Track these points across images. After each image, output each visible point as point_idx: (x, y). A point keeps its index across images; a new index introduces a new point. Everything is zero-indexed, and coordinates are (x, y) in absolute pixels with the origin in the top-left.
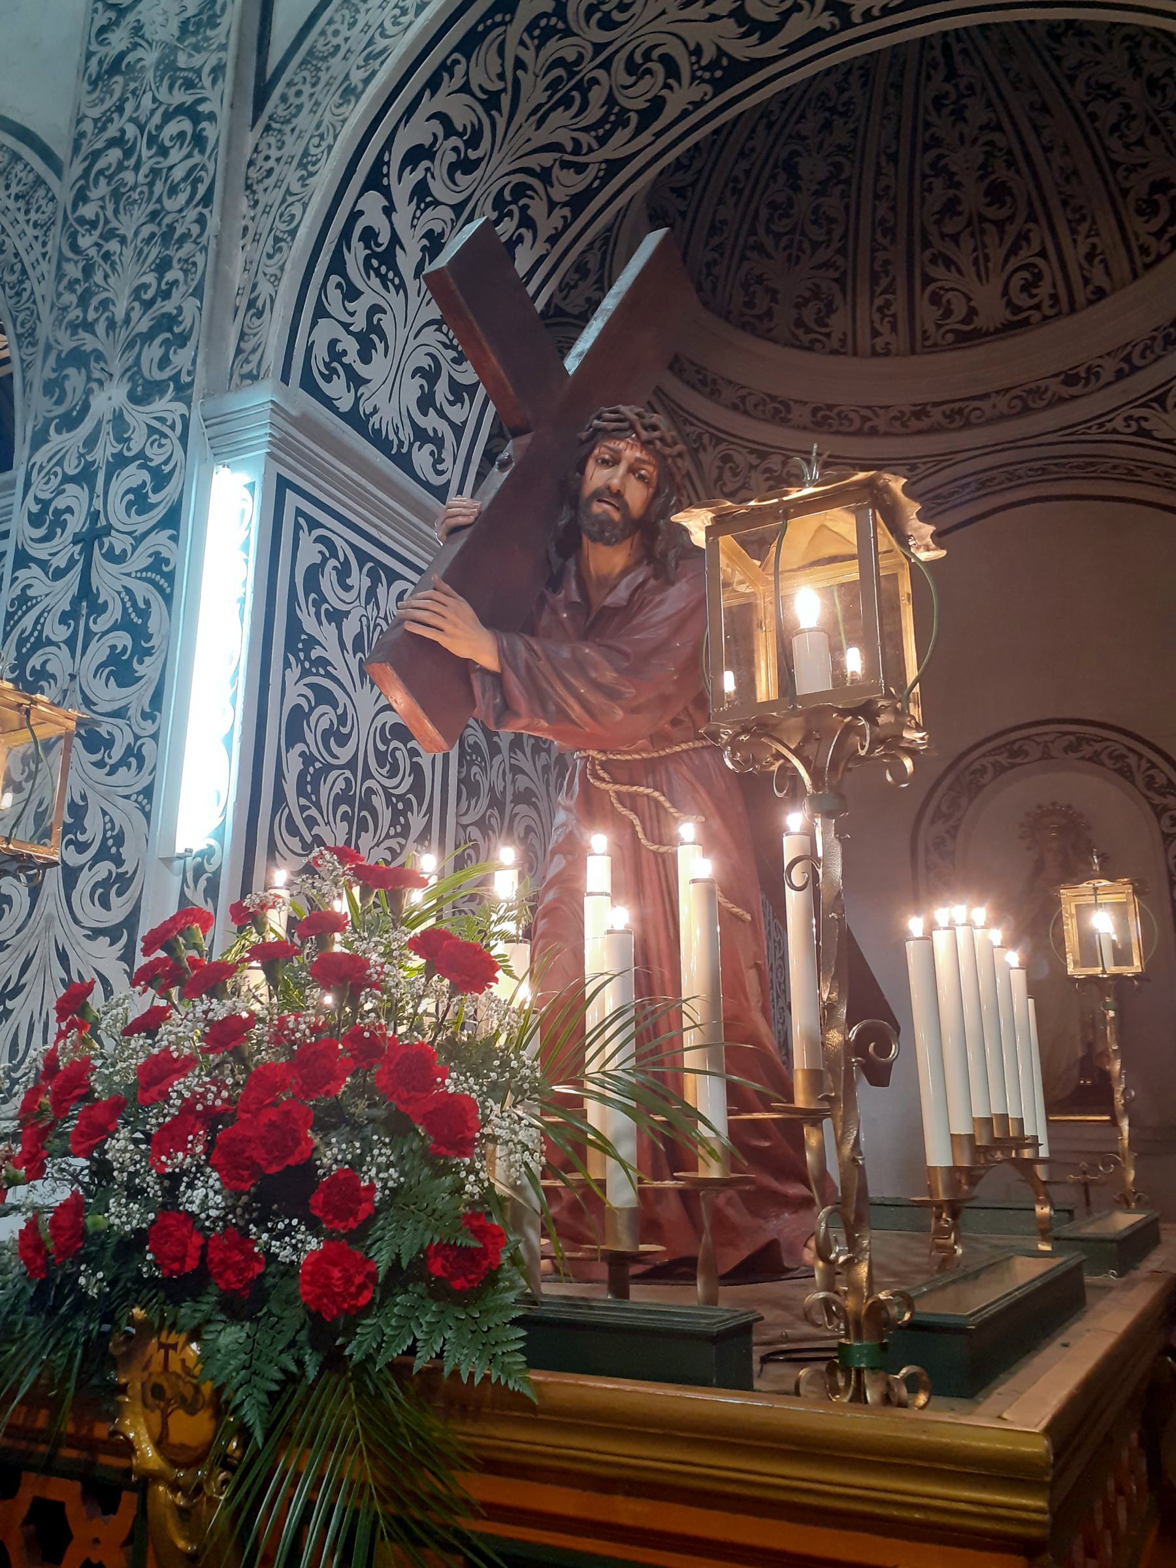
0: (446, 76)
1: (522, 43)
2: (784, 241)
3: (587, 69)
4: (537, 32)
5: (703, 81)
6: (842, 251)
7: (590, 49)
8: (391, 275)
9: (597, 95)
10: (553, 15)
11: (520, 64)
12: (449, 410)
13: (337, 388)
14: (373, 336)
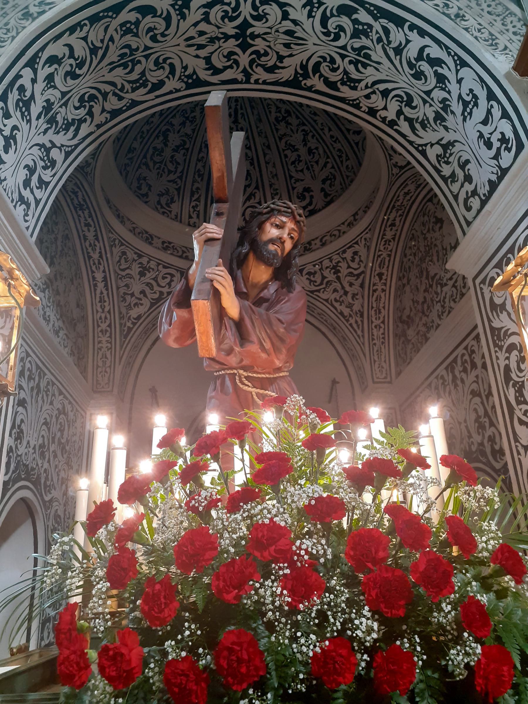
0: (79, 29)
1: (116, 30)
2: (157, 166)
3: (138, 55)
4: (124, 29)
5: (183, 81)
6: (180, 178)
7: (143, 47)
8: (26, 113)
9: (139, 69)
10: (133, 24)
11: (111, 39)
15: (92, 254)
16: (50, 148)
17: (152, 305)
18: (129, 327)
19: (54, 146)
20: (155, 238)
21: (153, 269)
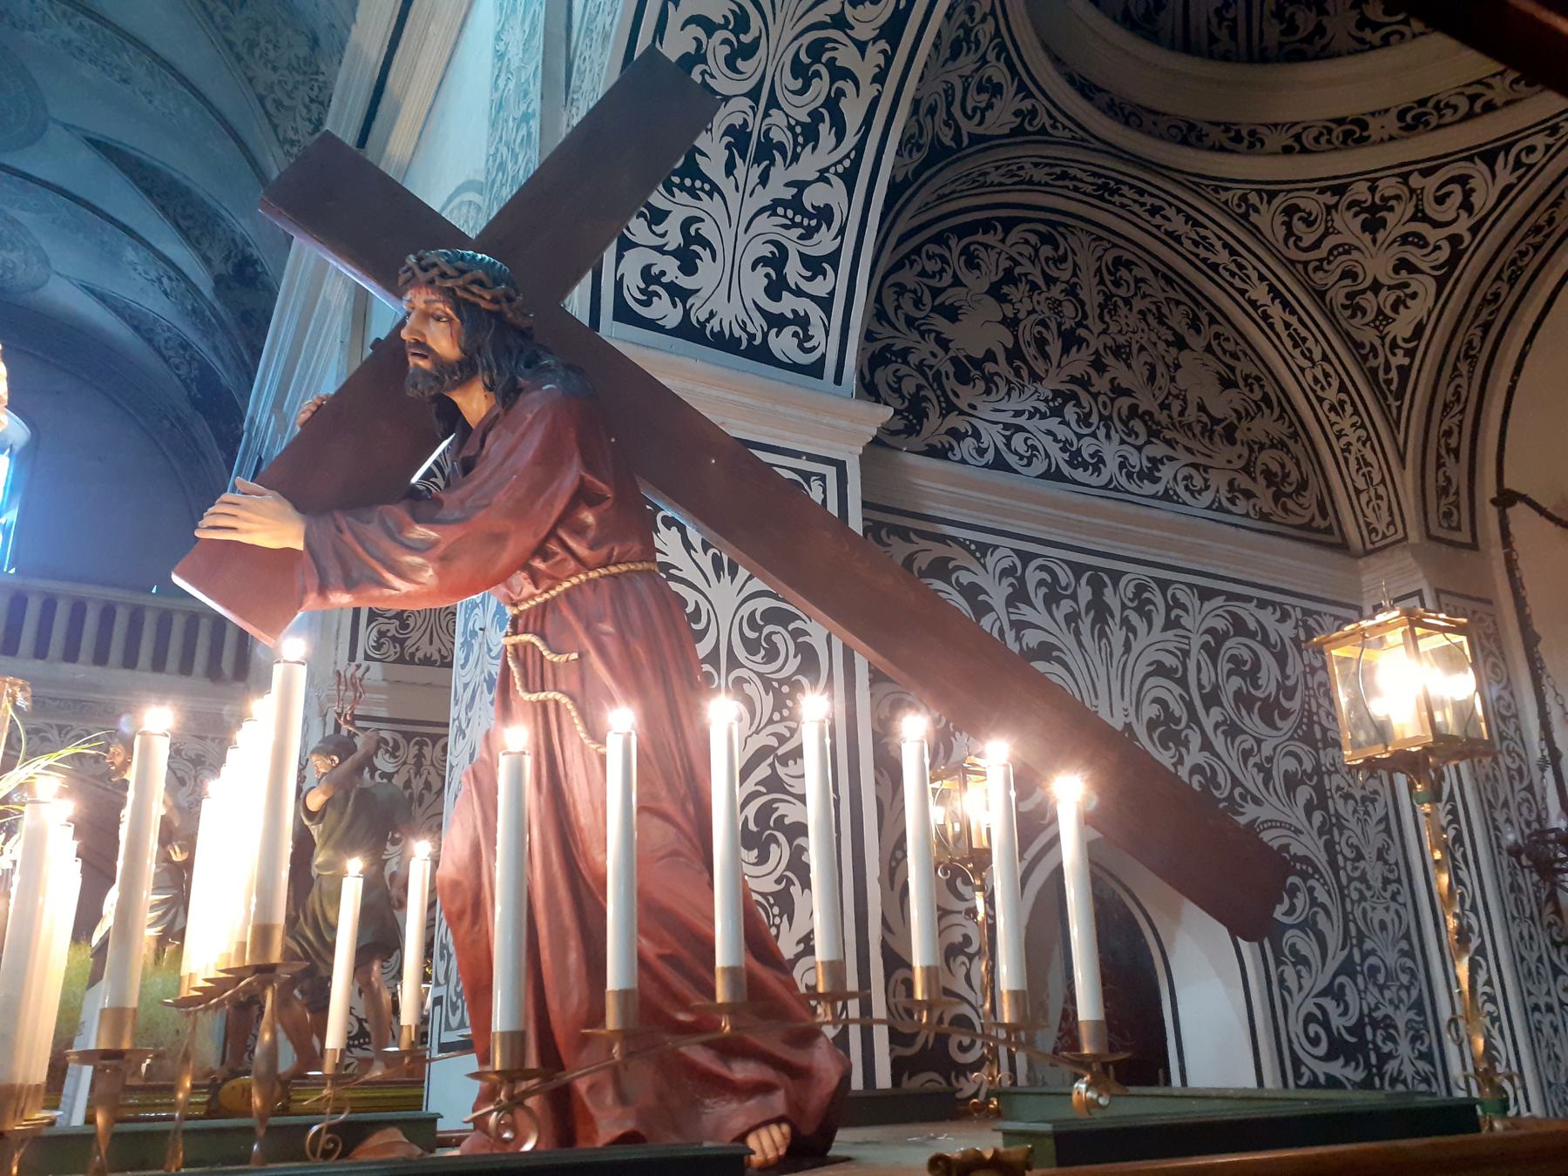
12: (806, 286)
13: (665, 310)
14: (694, 247)
15: (1213, 259)
16: (798, 197)
17: (1441, 283)
18: (1400, 368)
19: (801, 186)
20: (1369, 119)
21: (1397, 197)
